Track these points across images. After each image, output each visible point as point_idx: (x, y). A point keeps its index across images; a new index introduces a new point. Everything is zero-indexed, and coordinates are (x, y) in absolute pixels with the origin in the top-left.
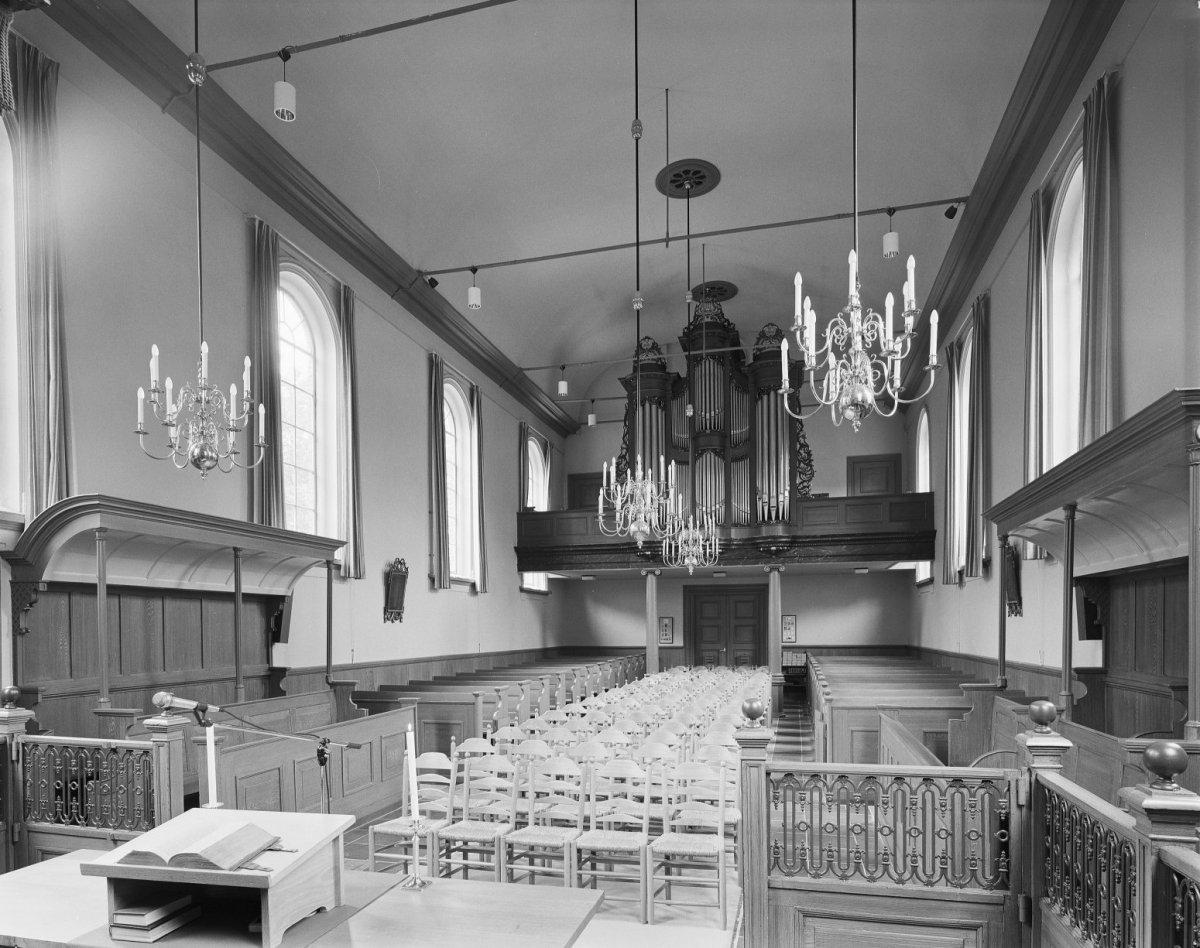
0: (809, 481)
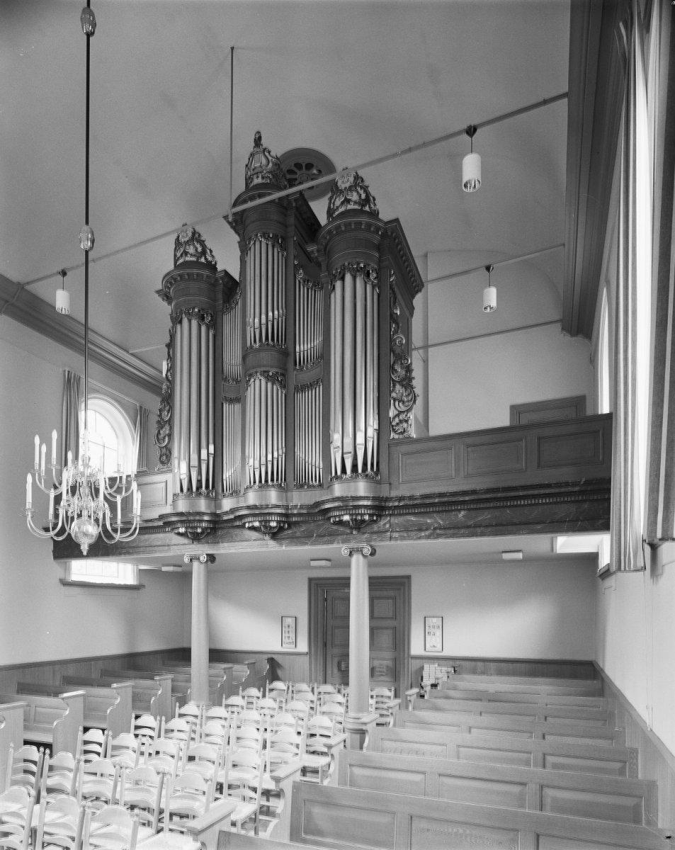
0: (408, 411)
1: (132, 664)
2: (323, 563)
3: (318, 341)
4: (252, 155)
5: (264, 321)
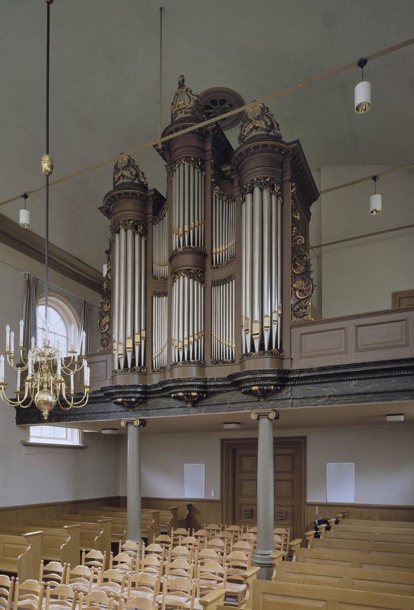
0: (308, 298)
1: (76, 509)
2: (234, 426)
3: (232, 243)
4: (177, 94)
5: (186, 229)
